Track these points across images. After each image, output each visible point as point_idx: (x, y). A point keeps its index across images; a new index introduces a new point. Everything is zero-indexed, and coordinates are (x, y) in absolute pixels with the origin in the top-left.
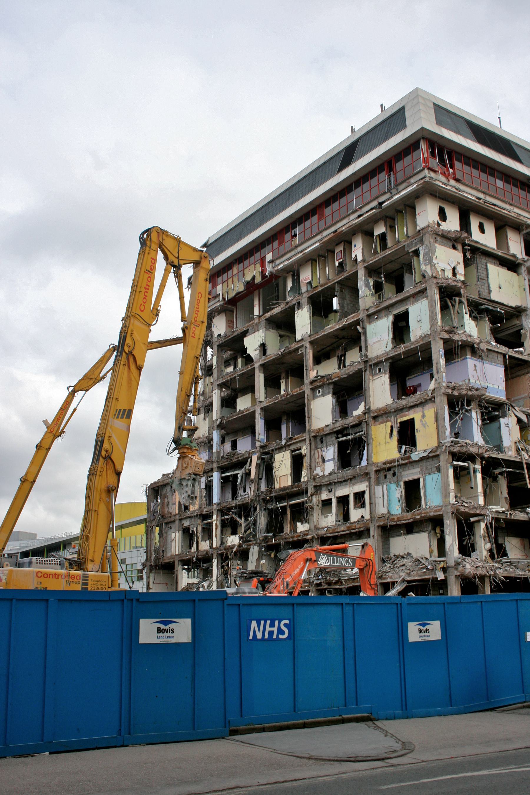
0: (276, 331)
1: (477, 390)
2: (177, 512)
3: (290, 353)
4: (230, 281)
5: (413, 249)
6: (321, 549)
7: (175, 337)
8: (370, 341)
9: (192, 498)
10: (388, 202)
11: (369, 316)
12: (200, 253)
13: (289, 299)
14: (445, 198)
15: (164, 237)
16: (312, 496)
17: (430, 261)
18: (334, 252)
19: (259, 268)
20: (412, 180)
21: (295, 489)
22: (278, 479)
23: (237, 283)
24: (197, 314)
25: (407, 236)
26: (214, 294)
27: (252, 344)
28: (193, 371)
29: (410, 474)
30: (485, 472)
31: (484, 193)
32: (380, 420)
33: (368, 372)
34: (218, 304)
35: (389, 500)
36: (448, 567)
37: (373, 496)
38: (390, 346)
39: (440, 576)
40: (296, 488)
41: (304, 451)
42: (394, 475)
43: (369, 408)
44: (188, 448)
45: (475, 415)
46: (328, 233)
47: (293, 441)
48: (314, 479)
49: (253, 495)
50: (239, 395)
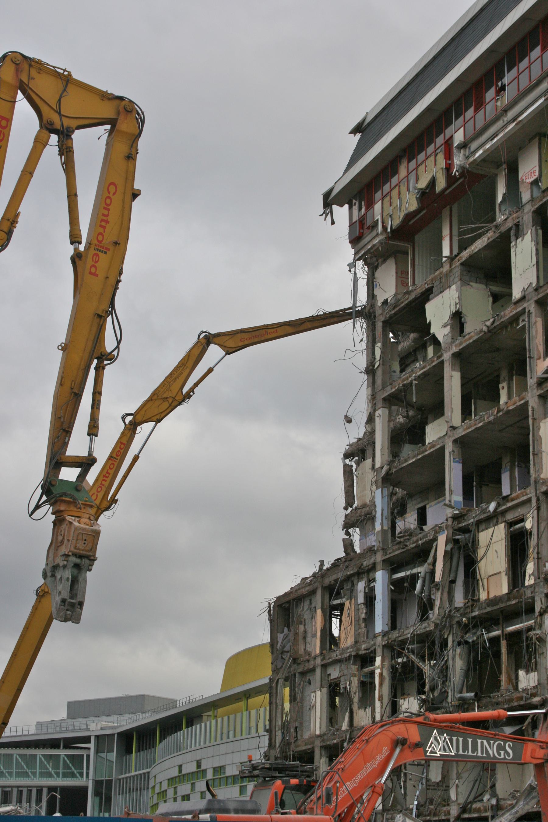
0: (483, 286)
2: (318, 651)
3: (504, 326)
4: (395, 193)
6: (435, 720)
7: (321, 313)
9: (72, 605)
12: (117, 102)
13: (500, 218)
15: (33, 72)
21: (513, 602)
22: (485, 581)
23: (406, 196)
24: (104, 227)
26: (369, 222)
27: (438, 314)
28: (90, 344)
34: (376, 241)
40: (514, 598)
41: (529, 524)
44: (69, 503)
47: (509, 504)
49: (439, 614)
50: (430, 417)
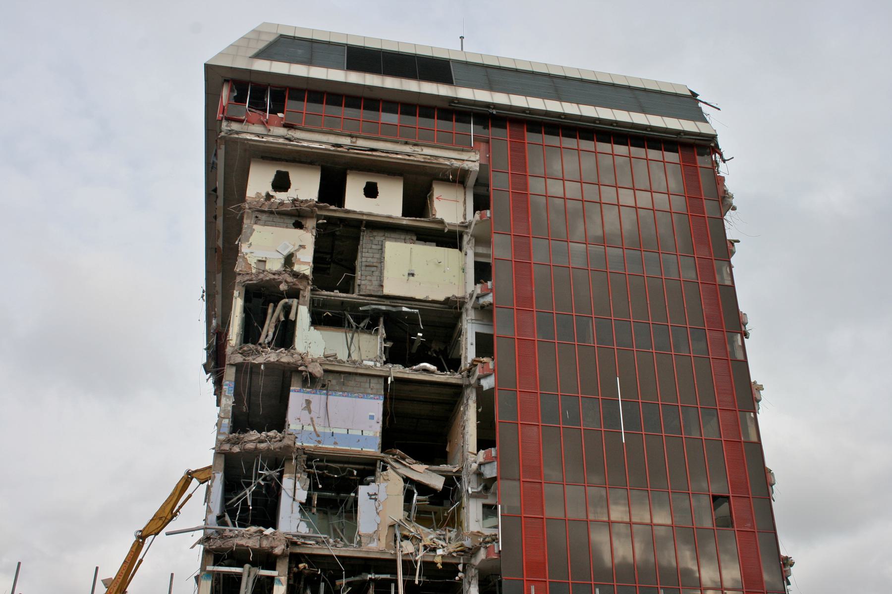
14: (286, 159)
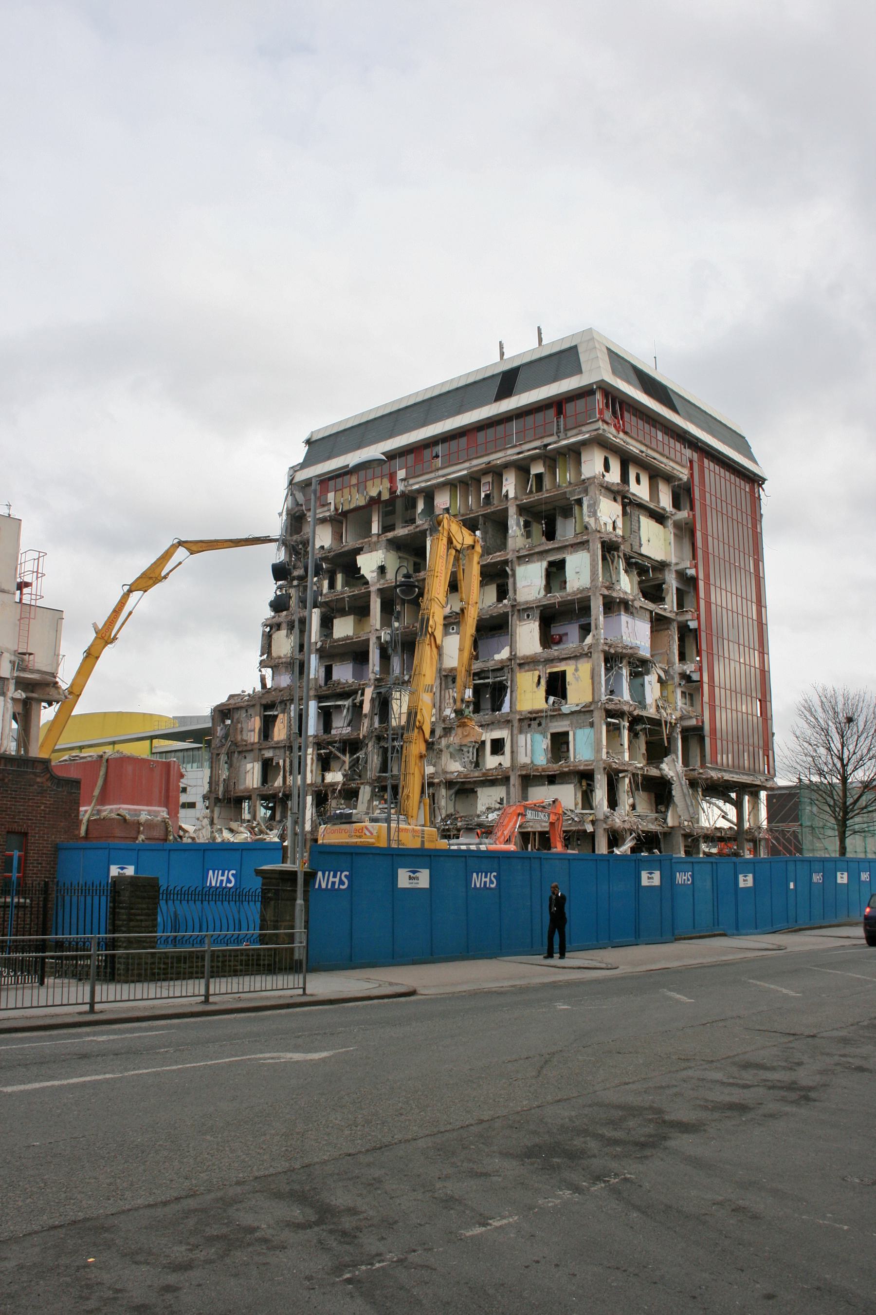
1: (631, 648)
4: (346, 491)
5: (576, 498)
8: (519, 584)
10: (555, 445)
11: (519, 558)
13: (419, 522)
16: (440, 737)
17: (594, 514)
18: (480, 482)
19: (387, 484)
20: (584, 429)
25: (570, 483)
27: (367, 564)
29: (559, 726)
30: (630, 729)
31: (646, 446)
32: (527, 668)
33: (515, 617)
34: (328, 514)
35: (533, 750)
36: (597, 820)
37: (515, 745)
38: (543, 593)
39: (590, 828)
42: (540, 724)
43: (515, 655)
45: (625, 672)
46: (479, 463)
48: (444, 721)
